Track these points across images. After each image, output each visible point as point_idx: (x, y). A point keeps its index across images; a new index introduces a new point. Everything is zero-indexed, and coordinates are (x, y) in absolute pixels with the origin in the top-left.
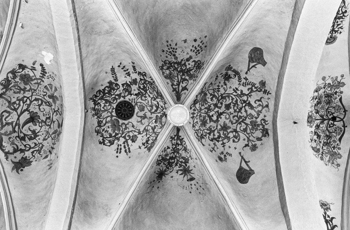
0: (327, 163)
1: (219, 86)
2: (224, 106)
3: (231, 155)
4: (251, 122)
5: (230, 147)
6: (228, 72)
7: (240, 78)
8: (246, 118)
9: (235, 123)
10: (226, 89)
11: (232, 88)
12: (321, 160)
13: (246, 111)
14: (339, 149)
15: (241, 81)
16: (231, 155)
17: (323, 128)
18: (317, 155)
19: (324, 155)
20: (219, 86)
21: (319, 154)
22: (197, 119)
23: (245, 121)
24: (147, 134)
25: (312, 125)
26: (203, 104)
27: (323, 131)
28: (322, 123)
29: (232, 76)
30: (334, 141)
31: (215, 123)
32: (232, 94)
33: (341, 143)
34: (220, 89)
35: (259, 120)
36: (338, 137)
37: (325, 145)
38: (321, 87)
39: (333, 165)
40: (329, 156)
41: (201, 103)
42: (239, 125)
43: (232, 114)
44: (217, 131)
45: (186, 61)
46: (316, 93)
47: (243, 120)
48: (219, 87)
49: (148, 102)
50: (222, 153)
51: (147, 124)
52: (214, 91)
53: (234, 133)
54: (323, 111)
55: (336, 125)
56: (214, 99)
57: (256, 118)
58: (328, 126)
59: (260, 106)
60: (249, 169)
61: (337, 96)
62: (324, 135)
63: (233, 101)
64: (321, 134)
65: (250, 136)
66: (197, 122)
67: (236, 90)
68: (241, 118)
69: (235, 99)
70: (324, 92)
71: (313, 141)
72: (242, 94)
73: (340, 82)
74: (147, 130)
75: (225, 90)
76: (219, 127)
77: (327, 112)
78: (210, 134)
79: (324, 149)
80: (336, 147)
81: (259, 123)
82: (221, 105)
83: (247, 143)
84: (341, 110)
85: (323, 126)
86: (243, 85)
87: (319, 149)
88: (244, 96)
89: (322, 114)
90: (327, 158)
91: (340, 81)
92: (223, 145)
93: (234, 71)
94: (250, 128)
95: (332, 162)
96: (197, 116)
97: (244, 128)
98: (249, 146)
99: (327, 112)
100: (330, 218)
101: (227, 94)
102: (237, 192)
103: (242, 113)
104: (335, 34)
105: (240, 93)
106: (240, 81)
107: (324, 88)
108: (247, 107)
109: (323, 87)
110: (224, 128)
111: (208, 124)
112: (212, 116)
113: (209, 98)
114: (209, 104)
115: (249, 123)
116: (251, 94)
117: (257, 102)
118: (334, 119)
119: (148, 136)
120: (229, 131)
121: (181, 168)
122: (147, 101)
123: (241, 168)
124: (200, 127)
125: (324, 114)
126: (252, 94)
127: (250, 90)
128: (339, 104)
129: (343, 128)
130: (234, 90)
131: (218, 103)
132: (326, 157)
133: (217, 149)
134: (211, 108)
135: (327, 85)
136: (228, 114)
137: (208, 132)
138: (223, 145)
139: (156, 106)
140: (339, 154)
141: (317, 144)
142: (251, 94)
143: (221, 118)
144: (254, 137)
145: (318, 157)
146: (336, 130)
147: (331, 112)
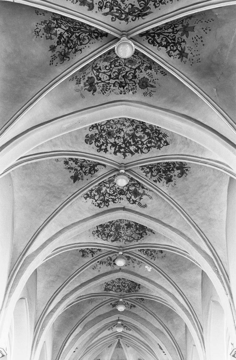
24: (111, 283)
49: (127, 282)
51: (116, 281)
74: (113, 282)
119: (111, 284)
122: (127, 281)
139: (125, 286)
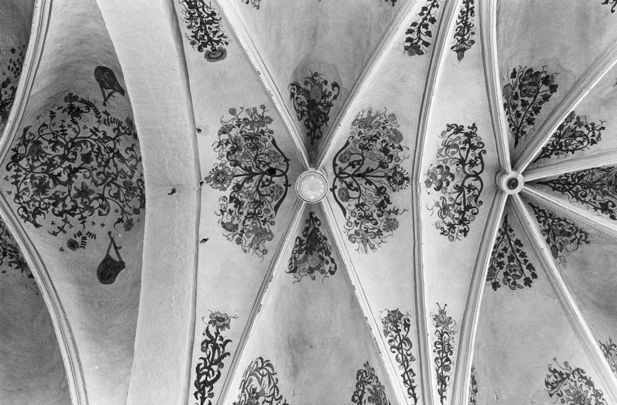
0: (247, 249)
1: (65, 127)
2: (81, 157)
3: (94, 236)
4: (124, 183)
5: (93, 223)
6: (72, 104)
7: (97, 113)
8: (116, 176)
9: (101, 185)
10: (78, 131)
11: (89, 128)
12: (237, 243)
13: (115, 165)
14: (271, 224)
15: (100, 117)
16: (94, 236)
17: (250, 189)
18: (230, 237)
19: (244, 234)
20: (65, 127)
21: (235, 234)
22: (26, 184)
23: (115, 181)
25: (225, 186)
26: (36, 158)
27: (249, 194)
28: (249, 179)
29: (84, 109)
30: (267, 211)
31: (66, 186)
32: (89, 137)
33: (277, 214)
34: (66, 130)
35: (134, 180)
36: (275, 203)
37: (250, 218)
38: (230, 125)
39: (258, 251)
40: (253, 236)
41: (30, 157)
42: (107, 187)
43: (96, 169)
44: (71, 198)
45: (2, 87)
46: (222, 135)
47: (113, 179)
48: (64, 128)
50: (80, 234)
52: (55, 135)
53: (100, 200)
54: (249, 160)
55: (274, 183)
56: (58, 147)
57: (131, 177)
58: (261, 184)
59: (133, 158)
60: (118, 260)
61: (267, 138)
62: (250, 200)
63: (93, 148)
64: (244, 199)
65: (124, 206)
66: (26, 189)
67: (94, 131)
68: (110, 177)
69: (96, 147)
70: (241, 132)
71: (225, 214)
72: (106, 138)
73: (263, 116)
75: (75, 131)
76: (73, 192)
77: (257, 162)
78: (55, 205)
79: (246, 224)
80: (268, 221)
81: (135, 185)
82: (74, 157)
83: (121, 217)
84: (280, 159)
85: (250, 186)
86: (105, 123)
87: (237, 225)
88: (109, 141)
89: (248, 165)
90: (249, 241)
91: (263, 114)
92: (82, 221)
93: (82, 101)
94: (124, 193)
95: (256, 245)
96: (25, 179)
97: (116, 192)
98: (123, 222)
99: (257, 162)
100: (222, 341)
101: (79, 138)
102: (87, 301)
103: (109, 168)
104: (219, 46)
105: (102, 136)
106: (98, 116)
107: (239, 127)
108: (116, 159)
109: (236, 125)
110: (83, 193)
111: (50, 189)
112: (59, 175)
113: (48, 147)
114: (50, 157)
115: (122, 185)
116: (119, 139)
117: (128, 151)
118: (272, 172)
120: (91, 197)
121: (13, 260)
123: (108, 258)
124: (35, 197)
125: (251, 166)
126: (121, 137)
127: (116, 132)
128: (274, 148)
129: (284, 187)
130: (91, 131)
131: (68, 153)
132: (246, 238)
133: (70, 228)
134: (54, 163)
135: (241, 120)
136: (89, 170)
137: (51, 202)
138: (82, 221)
140: (270, 233)
141: (233, 218)
142: (120, 137)
143: (76, 177)
144: (130, 208)
145: (231, 238)
146: (272, 192)
147: (264, 161)
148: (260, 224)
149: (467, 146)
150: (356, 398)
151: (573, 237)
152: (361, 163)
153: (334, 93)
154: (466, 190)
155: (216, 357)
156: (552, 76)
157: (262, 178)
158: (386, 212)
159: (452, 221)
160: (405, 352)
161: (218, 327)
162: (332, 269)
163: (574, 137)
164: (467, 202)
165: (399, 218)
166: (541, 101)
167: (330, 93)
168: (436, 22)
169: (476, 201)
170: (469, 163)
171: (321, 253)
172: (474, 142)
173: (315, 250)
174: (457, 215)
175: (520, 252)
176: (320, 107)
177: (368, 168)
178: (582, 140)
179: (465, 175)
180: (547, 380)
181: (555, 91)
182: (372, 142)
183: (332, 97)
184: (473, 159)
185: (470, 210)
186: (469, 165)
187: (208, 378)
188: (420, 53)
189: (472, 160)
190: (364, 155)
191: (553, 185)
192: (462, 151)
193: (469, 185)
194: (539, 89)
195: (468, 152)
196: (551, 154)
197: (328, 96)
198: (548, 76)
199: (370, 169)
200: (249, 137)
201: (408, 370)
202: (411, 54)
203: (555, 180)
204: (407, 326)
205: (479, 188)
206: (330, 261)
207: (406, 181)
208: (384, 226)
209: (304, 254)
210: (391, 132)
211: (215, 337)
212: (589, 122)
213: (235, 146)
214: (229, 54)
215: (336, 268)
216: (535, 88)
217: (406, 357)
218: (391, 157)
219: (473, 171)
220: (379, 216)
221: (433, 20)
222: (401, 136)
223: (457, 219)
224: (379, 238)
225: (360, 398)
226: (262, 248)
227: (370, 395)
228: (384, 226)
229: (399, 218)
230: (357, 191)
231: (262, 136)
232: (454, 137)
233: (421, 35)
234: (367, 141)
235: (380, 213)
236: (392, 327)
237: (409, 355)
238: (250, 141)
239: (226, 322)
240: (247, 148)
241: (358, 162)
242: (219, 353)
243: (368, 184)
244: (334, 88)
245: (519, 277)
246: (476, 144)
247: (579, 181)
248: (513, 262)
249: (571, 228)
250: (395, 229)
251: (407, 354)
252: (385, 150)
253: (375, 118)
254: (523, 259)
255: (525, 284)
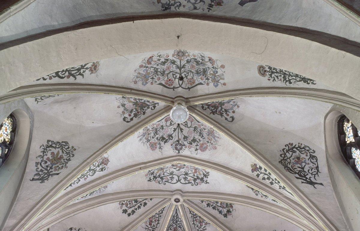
0: (137, 72)
12: (140, 66)
14: (151, 83)
17: (172, 68)
18: (144, 61)
19: (145, 68)
30: (159, 79)
36: (163, 83)
37: (155, 70)
39: (136, 78)
46: (208, 59)
54: (190, 68)
61: (204, 81)
70: (209, 68)
77: (188, 72)
84: (190, 85)
85: (174, 68)
87: (151, 64)
89: (186, 67)
90: (142, 72)
100: (83, 73)
104: (268, 75)
129: (172, 87)
135: (216, 70)
140: (146, 83)
141: (155, 61)
145: (143, 62)
147: (188, 75)
148: (151, 76)
149: (195, 177)
150: (50, 143)
151: (149, 226)
152: (186, 126)
153: (228, 118)
154: (171, 176)
155: (73, 72)
156: (231, 214)
157: (178, 73)
158: (159, 142)
159: (155, 173)
160: (88, 174)
161: (91, 68)
162: (126, 119)
163: (200, 222)
164: (165, 177)
165: (157, 150)
166: (219, 209)
167: (228, 115)
168: (271, 185)
169: (166, 181)
170: (186, 177)
171: (134, 110)
172: (198, 181)
173: (136, 106)
174: (158, 174)
175: (140, 206)
176: (220, 108)
177: (183, 130)
178: (199, 226)
179: (179, 175)
180: (73, 228)
181: (224, 217)
182: (199, 134)
183: (226, 117)
184: (188, 179)
185: (161, 180)
186: (185, 177)
187: (61, 72)
188: (253, 171)
189: (187, 179)
190: (190, 128)
191: (176, 215)
192: (193, 174)
193: (174, 177)
194: (224, 208)
195: (192, 177)
196: (192, 214)
197: (226, 114)
198: (231, 212)
199: (182, 130)
200: (205, 71)
201: (79, 179)
202: (252, 166)
203: (178, 216)
204: (102, 170)
205: (172, 182)
206: (131, 117)
207: (178, 152)
208: (152, 142)
209: (133, 101)
210: (205, 145)
211: (85, 68)
212: (207, 228)
213: (199, 63)
214: (262, 78)
215: (128, 122)
216: (225, 206)
217: (85, 175)
218: (191, 144)
219: (181, 179)
220: (157, 138)
221: (272, 183)
222: (204, 151)
223: (156, 175)
224: (146, 141)
225: (51, 146)
226: (137, 80)
227: (56, 154)
228: (152, 142)
229: (157, 150)
230: (170, 124)
231: (205, 78)
232: (202, 173)
233: (263, 175)
234: (200, 131)
235: (159, 138)
236: (100, 162)
237: (87, 177)
238: (202, 71)
239: (94, 71)
240: (197, 68)
241: (187, 125)
242: (75, 73)
243: (174, 129)
244: (231, 118)
245: (127, 206)
246: (196, 181)
247: (178, 226)
248: (135, 203)
249: (154, 226)
250: (151, 149)
251: (87, 175)
252: (194, 140)
253: (215, 139)
254: (137, 208)
255: (123, 210)
